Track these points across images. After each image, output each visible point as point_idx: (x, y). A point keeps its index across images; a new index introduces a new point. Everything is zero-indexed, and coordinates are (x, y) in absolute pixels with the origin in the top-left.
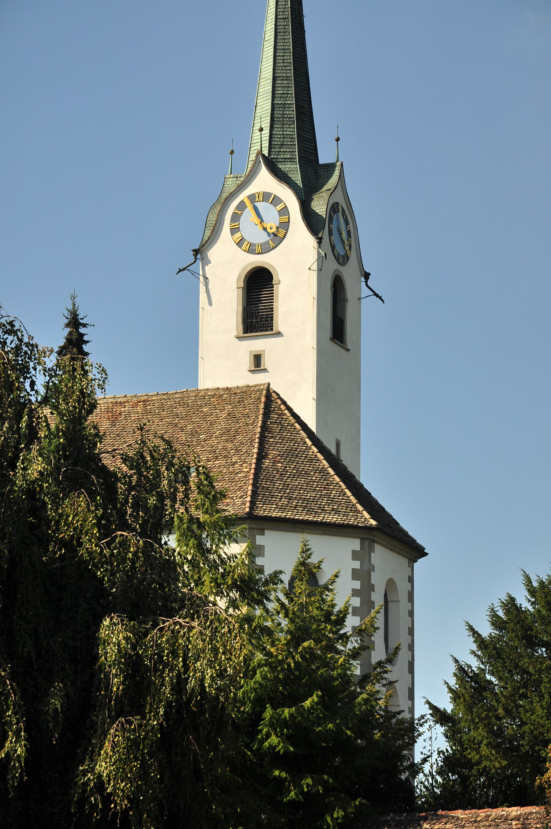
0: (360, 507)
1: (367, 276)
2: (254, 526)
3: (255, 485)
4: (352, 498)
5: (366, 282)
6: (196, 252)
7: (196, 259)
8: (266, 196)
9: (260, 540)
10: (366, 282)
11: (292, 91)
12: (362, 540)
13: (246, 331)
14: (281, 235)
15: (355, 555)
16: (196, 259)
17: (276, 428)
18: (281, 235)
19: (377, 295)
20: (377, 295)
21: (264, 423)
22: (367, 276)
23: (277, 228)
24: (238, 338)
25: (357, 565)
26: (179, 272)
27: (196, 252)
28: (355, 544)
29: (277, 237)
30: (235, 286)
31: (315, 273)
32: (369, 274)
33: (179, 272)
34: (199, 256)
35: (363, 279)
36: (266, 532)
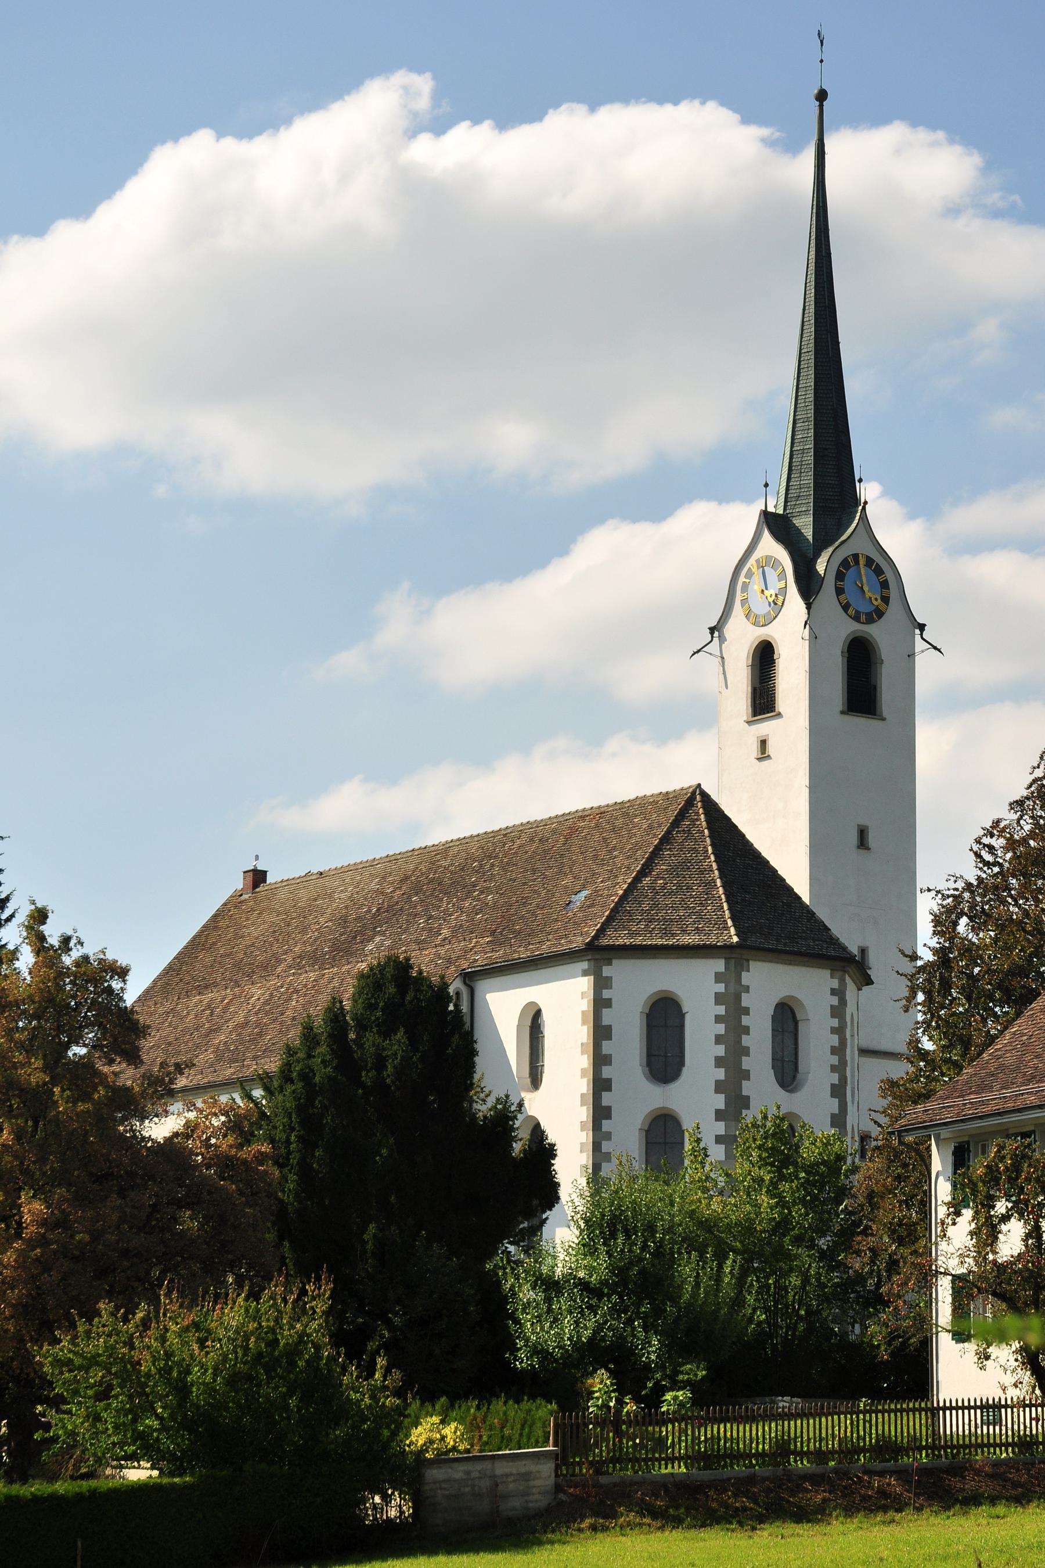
0: (730, 923)
1: (922, 627)
2: (597, 957)
3: (615, 911)
4: (727, 912)
5: (921, 635)
6: (712, 630)
9: (606, 971)
10: (921, 635)
11: (811, 433)
15: (719, 978)
17: (680, 837)
19: (935, 648)
20: (935, 648)
22: (922, 627)
23: (776, 595)
24: (749, 723)
25: (721, 988)
27: (712, 630)
28: (719, 965)
29: (777, 606)
31: (807, 642)
34: (716, 634)
35: (917, 631)
36: (614, 962)
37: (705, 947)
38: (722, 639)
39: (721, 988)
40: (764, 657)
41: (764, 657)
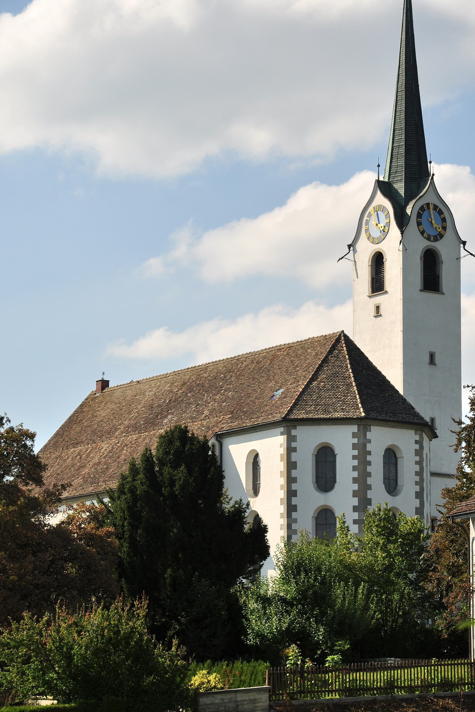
0: (360, 405)
1: (464, 243)
2: (288, 425)
5: (464, 247)
6: (349, 246)
7: (349, 250)
8: (380, 206)
9: (294, 432)
10: (464, 247)
11: (403, 136)
12: (359, 425)
13: (373, 292)
14: (386, 231)
16: (349, 250)
17: (332, 360)
18: (386, 231)
19: (471, 254)
20: (471, 254)
21: (326, 357)
22: (464, 243)
24: (370, 297)
25: (355, 441)
26: (339, 260)
27: (349, 246)
28: (354, 428)
30: (367, 265)
32: (466, 242)
33: (339, 260)
34: (352, 248)
35: (462, 245)
36: (298, 427)
37: (347, 419)
38: (355, 251)
39: (355, 441)
40: (378, 260)
41: (378, 260)
